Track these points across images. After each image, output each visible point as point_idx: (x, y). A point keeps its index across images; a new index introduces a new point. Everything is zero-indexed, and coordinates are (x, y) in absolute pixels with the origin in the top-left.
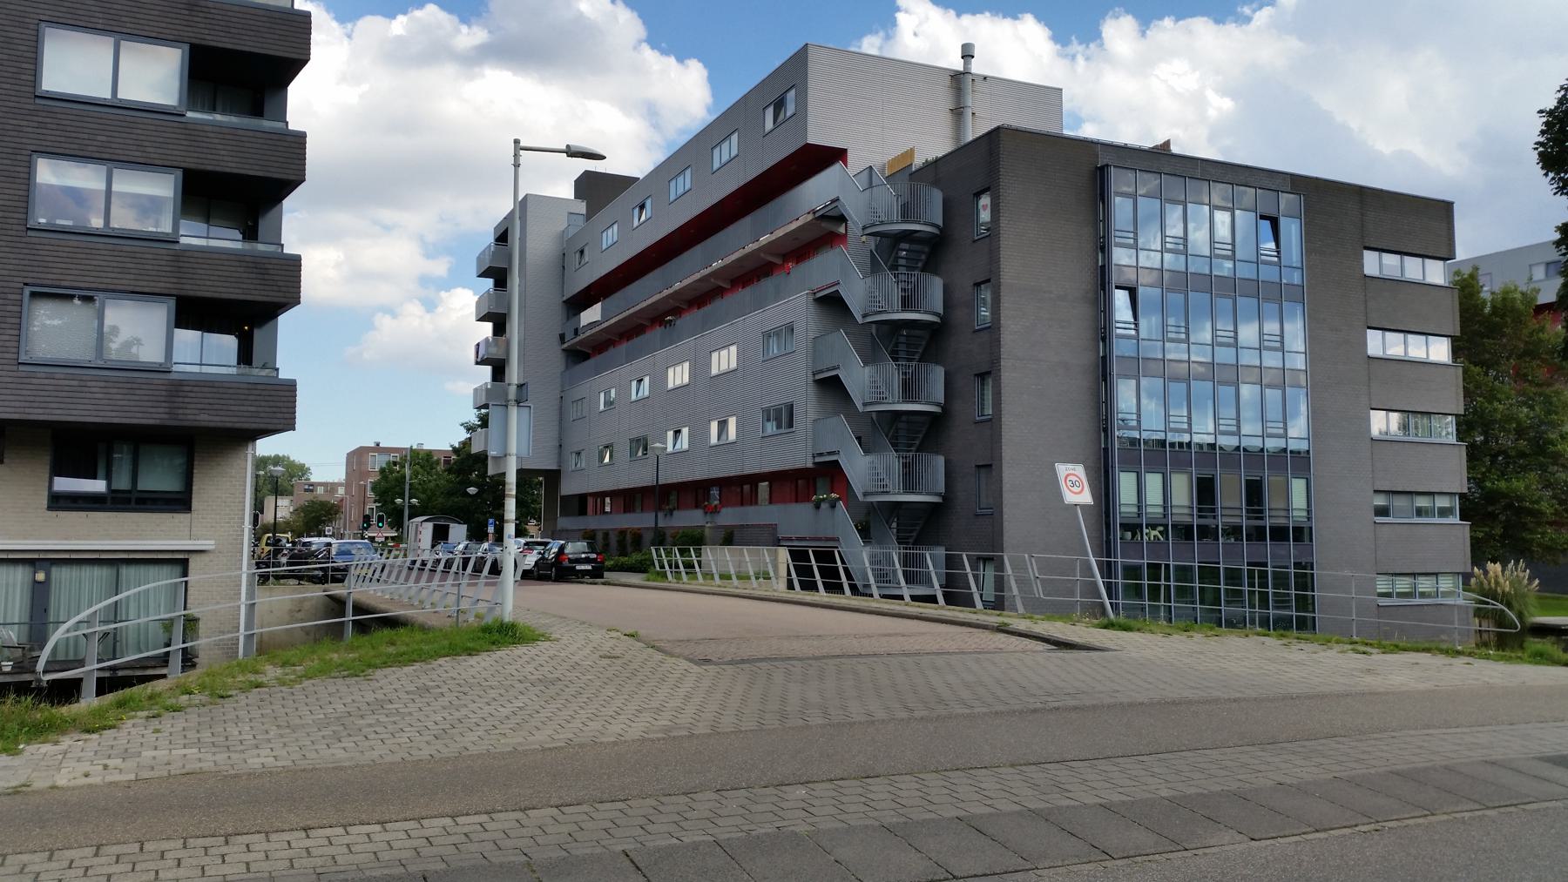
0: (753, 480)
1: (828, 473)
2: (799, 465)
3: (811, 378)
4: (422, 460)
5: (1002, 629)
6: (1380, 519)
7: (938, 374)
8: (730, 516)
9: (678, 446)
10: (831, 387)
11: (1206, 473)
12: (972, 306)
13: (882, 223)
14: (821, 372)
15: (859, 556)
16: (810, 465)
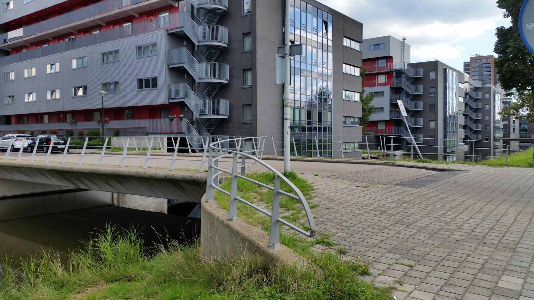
0: (42, 115)
1: (177, 108)
2: (164, 103)
3: (167, 67)
4: (497, 43)
5: (394, 165)
6: (344, 125)
7: (227, 68)
8: (114, 124)
9: (53, 97)
10: (179, 73)
11: (310, 109)
12: (241, 43)
13: (205, 4)
14: (171, 65)
15: (193, 137)
16: (167, 103)
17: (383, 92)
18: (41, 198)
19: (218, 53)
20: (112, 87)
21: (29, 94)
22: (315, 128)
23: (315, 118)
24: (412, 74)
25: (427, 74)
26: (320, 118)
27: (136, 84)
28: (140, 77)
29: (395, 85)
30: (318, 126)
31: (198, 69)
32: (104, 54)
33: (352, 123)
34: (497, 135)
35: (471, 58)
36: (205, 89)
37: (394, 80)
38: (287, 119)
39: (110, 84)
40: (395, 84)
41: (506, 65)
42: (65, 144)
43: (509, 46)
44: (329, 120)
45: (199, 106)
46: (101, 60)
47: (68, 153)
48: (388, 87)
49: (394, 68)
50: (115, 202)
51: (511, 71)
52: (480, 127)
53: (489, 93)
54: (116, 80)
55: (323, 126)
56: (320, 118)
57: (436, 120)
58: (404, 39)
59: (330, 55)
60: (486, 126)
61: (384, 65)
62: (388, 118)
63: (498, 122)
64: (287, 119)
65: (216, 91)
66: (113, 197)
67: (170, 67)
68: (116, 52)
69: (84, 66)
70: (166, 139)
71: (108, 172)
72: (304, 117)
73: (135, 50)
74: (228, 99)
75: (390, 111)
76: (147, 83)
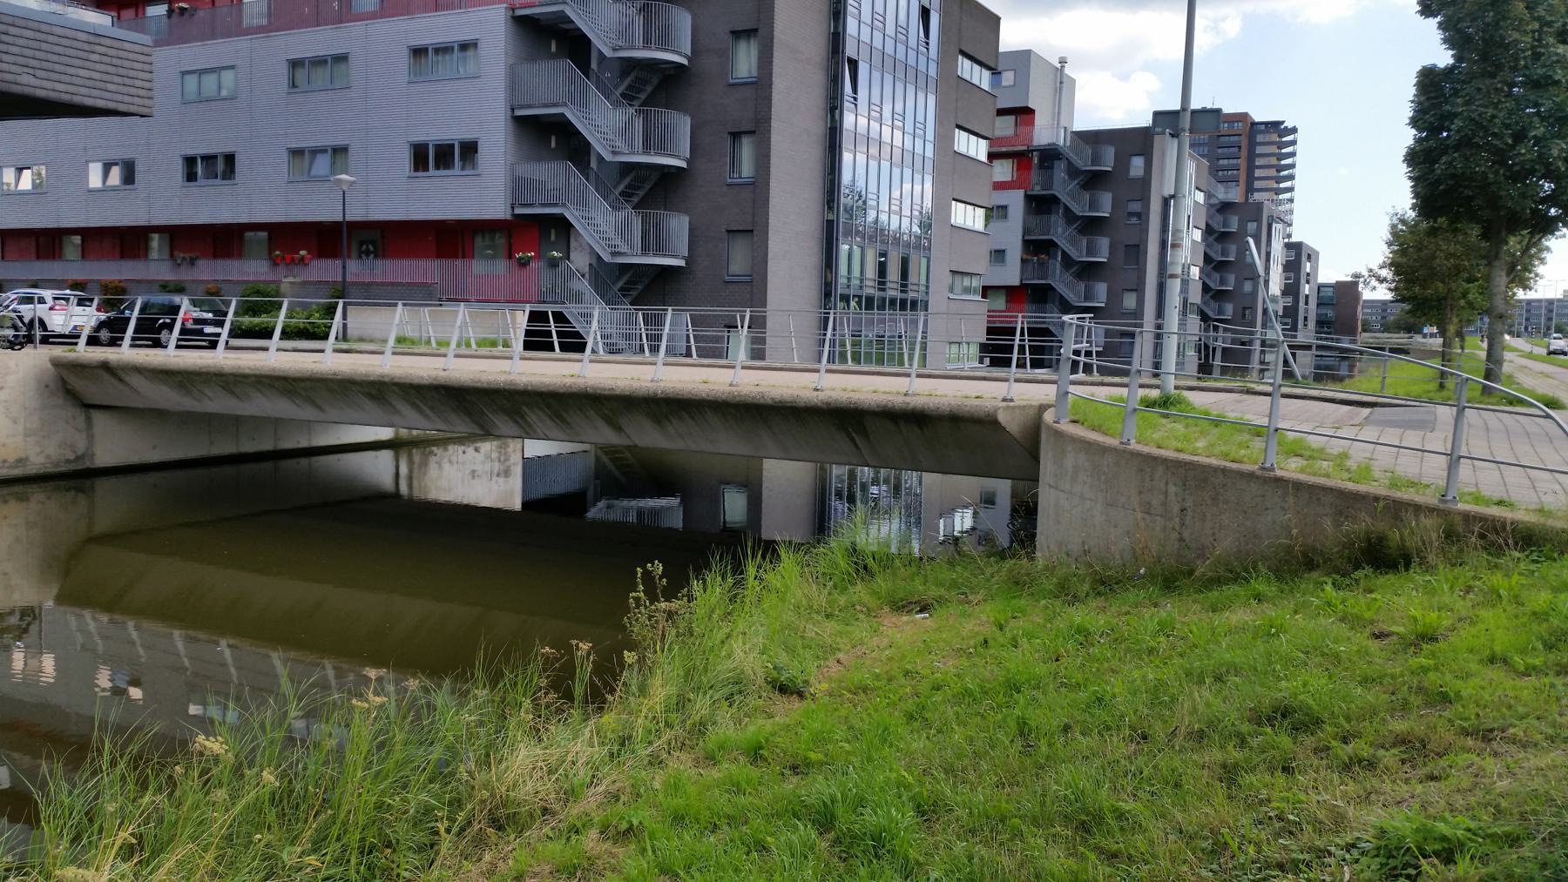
1: (531, 232)
8: (356, 269)
10: (547, 134)
12: (727, 57)
14: (522, 107)
16: (509, 217)
17: (1004, 208)
18: (228, 470)
19: (655, 81)
20: (322, 164)
21: (20, 170)
22: (893, 302)
23: (893, 274)
24: (1083, 163)
25: (1122, 161)
26: (904, 274)
27: (405, 159)
28: (420, 138)
29: (1037, 190)
30: (877, 294)
31: (607, 126)
32: (295, 64)
33: (967, 290)
34: (1271, 335)
35: (1157, 114)
36: (619, 183)
37: (1035, 176)
38: (1173, 276)
39: (315, 152)
40: (1038, 188)
41: (1444, 159)
42: (221, 324)
43: (1456, 115)
44: (923, 281)
45: (603, 229)
46: (285, 80)
47: (228, 347)
48: (1021, 192)
49: (1035, 143)
50: (404, 489)
51: (1454, 176)
52: (1229, 309)
53: (1258, 220)
54: (339, 141)
55: (911, 295)
56: (904, 274)
57: (1139, 289)
58: (1063, 61)
59: (932, 99)
60: (1245, 309)
61: (1010, 132)
62: (1014, 280)
63: (1274, 300)
64: (1173, 276)
65: (651, 189)
66: (397, 475)
67: (519, 113)
68: (342, 58)
69: (224, 93)
70: (522, 319)
71: (641, 393)
72: (871, 272)
73: (404, 57)
74: (686, 212)
75: (1023, 261)
76: (433, 157)
